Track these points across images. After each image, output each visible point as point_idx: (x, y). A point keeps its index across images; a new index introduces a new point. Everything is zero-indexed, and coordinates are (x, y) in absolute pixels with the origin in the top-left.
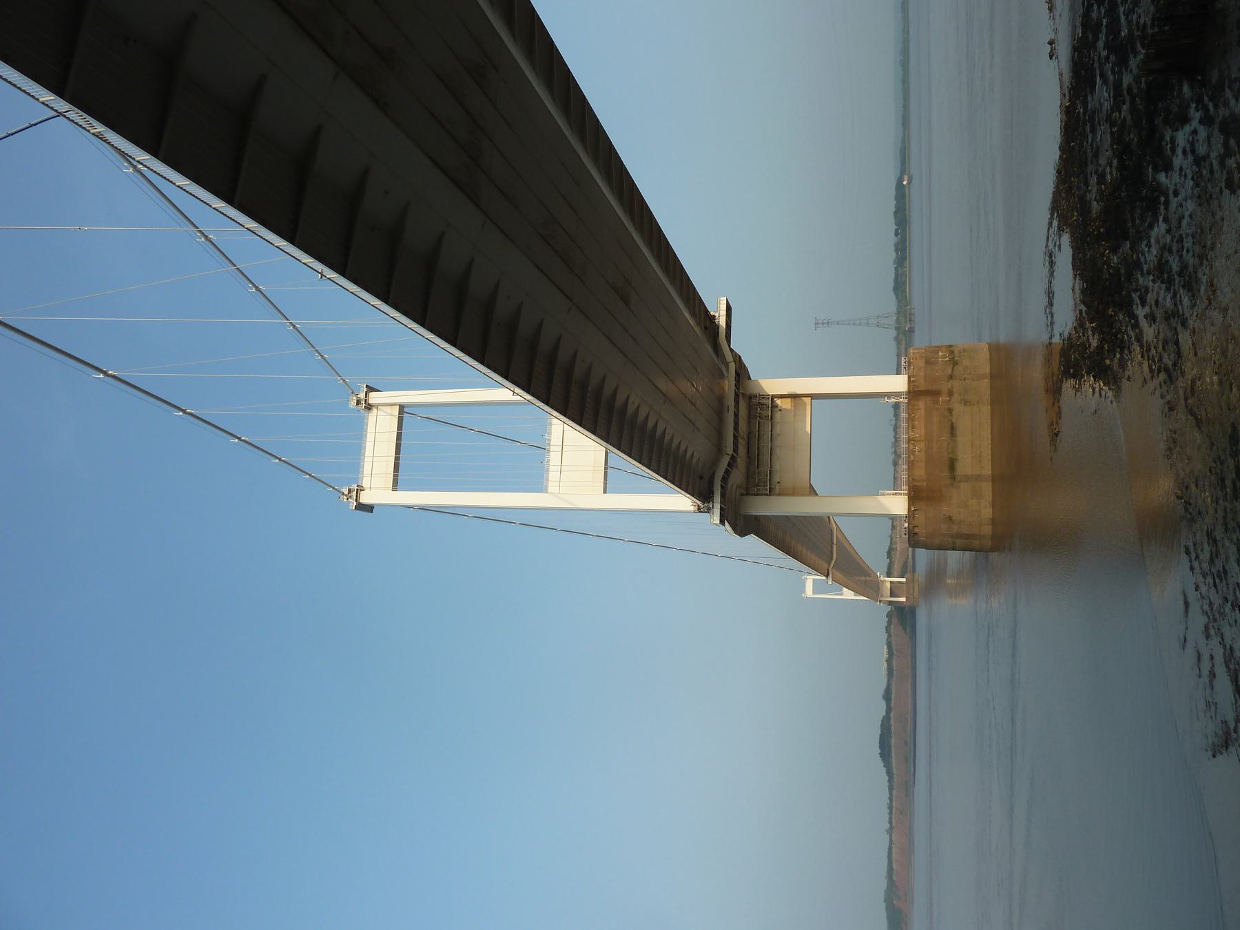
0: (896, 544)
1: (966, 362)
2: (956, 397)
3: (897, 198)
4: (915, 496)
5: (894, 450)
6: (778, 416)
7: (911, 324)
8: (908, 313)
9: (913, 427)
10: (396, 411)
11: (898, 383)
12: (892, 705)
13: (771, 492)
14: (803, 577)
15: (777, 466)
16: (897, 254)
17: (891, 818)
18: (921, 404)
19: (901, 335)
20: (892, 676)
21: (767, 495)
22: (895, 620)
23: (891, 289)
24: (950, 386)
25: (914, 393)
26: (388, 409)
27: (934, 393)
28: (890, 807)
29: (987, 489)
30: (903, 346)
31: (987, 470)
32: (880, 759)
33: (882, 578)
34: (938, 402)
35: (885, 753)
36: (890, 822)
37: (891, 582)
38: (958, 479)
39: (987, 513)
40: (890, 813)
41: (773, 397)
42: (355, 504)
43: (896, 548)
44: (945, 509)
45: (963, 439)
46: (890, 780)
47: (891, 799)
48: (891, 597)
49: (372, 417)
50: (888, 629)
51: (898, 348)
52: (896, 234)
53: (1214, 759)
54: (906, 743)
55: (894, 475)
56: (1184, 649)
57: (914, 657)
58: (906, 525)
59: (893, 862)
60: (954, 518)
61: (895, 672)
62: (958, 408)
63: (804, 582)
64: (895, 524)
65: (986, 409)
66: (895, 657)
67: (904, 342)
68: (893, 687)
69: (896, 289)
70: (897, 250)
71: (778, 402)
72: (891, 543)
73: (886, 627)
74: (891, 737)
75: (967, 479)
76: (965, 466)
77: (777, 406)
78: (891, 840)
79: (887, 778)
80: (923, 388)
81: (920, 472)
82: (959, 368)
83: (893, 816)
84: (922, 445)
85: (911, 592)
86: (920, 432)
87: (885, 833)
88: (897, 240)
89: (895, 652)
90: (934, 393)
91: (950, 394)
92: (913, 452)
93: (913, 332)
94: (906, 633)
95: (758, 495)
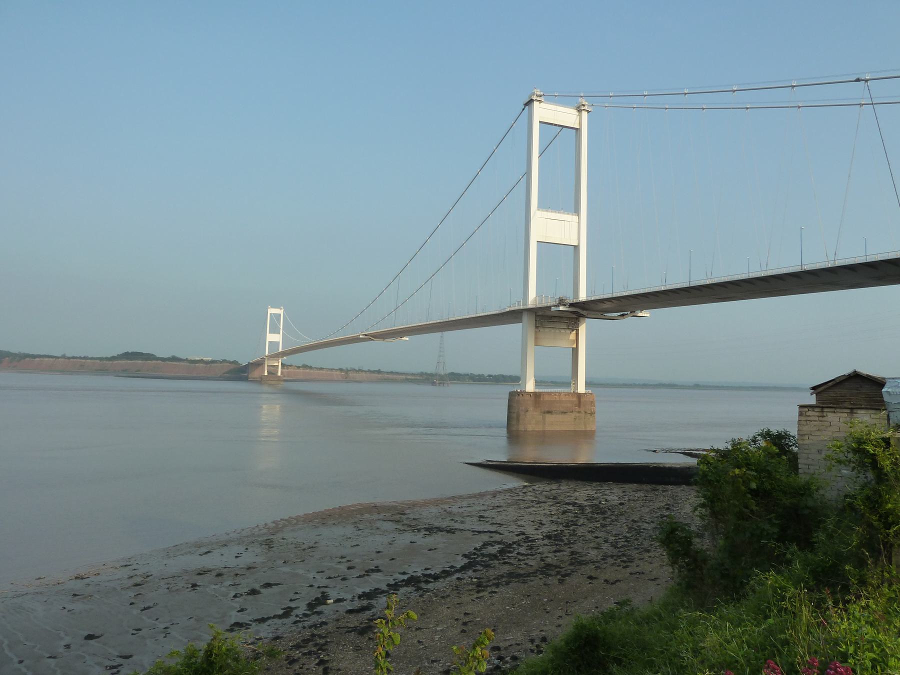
0: (288, 369)
1: (591, 419)
2: (578, 415)
3: (510, 376)
4: (536, 395)
5: (349, 369)
6: (568, 331)
7: (438, 383)
8: (445, 382)
9: (565, 395)
10: (577, 126)
11: (581, 389)
12: (168, 362)
13: (537, 327)
14: (282, 307)
15: (547, 330)
16: (477, 376)
17: (76, 358)
18: (575, 399)
19: (426, 376)
20: (190, 363)
21: (536, 325)
22: (233, 366)
23: (453, 371)
24: (582, 412)
25: (579, 396)
26: (578, 122)
27: (579, 405)
28: (85, 358)
29: (539, 428)
30: (418, 378)
31: (548, 428)
32: (124, 352)
33: (280, 361)
34: (576, 407)
35: (127, 356)
36: (74, 358)
37: (278, 366)
38: (544, 415)
39: (530, 428)
40: (80, 358)
41: (577, 330)
42: (534, 99)
43: (284, 369)
44: (531, 409)
45: (560, 417)
46: (107, 359)
47: (92, 358)
48: (268, 366)
49: (575, 112)
50: (224, 361)
51: (417, 374)
52: (489, 376)
53: (234, 558)
54: (139, 371)
55: (334, 369)
56: (76, 578)
57: (208, 379)
58: (519, 391)
59: (41, 359)
60: (527, 413)
61: (193, 365)
62: (573, 415)
63: (279, 307)
64: (334, 370)
65: (572, 428)
66: (205, 365)
67: (421, 378)
68: (182, 363)
69: (452, 374)
70: (479, 375)
71: (574, 332)
72: (288, 365)
73: (225, 360)
74: (142, 361)
75: (544, 419)
76: (549, 418)
77: (573, 331)
78: (58, 358)
79: (109, 357)
80: (581, 400)
81: (547, 398)
82: (589, 416)
83: (79, 360)
84: (558, 399)
85: (271, 379)
86: (563, 398)
87: (63, 354)
88: (486, 376)
89: (208, 365)
90: (579, 405)
91: (579, 412)
92: (555, 395)
93: (433, 385)
94: (224, 373)
95: (536, 320)
